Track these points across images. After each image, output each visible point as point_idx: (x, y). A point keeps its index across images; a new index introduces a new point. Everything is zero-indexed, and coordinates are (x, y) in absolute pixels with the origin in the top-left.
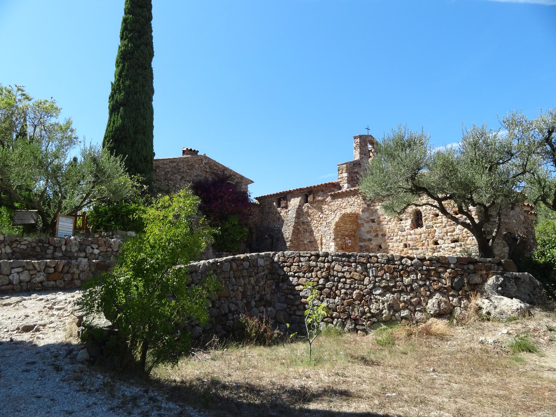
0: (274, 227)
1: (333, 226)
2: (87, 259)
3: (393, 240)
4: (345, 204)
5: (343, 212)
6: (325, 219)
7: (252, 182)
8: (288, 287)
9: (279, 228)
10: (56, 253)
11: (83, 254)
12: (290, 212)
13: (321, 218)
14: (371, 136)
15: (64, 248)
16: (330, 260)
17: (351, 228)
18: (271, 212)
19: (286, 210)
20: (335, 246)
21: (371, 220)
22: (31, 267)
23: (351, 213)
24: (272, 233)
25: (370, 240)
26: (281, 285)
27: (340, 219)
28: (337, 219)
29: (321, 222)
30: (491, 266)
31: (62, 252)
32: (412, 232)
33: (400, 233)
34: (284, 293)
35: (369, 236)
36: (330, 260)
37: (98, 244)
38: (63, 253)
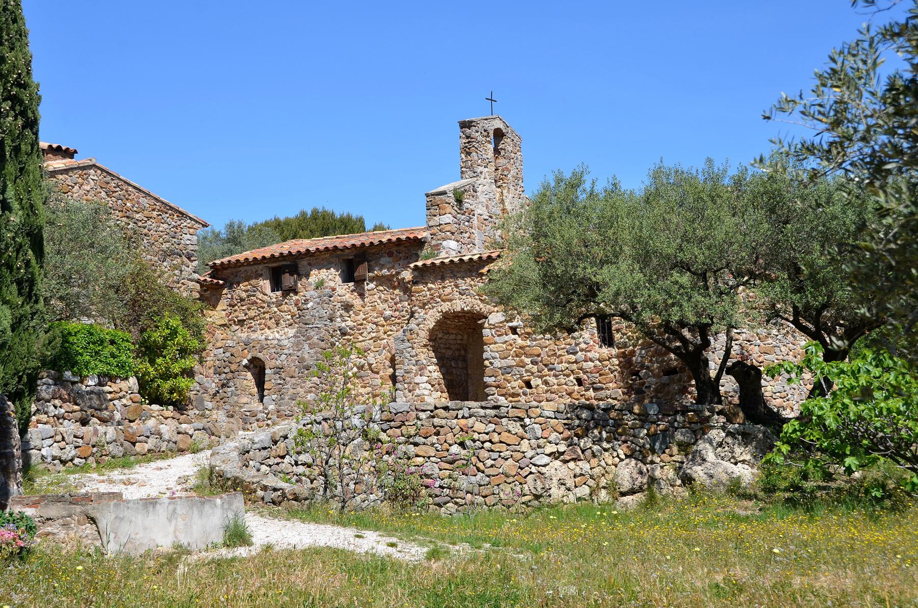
0: (266, 339)
5: (446, 307)
12: (310, 305)
13: (386, 319)
17: (459, 342)
19: (295, 298)
21: (511, 328)
24: (260, 355)
27: (439, 323)
28: (431, 325)
29: (388, 328)
36: (466, 415)
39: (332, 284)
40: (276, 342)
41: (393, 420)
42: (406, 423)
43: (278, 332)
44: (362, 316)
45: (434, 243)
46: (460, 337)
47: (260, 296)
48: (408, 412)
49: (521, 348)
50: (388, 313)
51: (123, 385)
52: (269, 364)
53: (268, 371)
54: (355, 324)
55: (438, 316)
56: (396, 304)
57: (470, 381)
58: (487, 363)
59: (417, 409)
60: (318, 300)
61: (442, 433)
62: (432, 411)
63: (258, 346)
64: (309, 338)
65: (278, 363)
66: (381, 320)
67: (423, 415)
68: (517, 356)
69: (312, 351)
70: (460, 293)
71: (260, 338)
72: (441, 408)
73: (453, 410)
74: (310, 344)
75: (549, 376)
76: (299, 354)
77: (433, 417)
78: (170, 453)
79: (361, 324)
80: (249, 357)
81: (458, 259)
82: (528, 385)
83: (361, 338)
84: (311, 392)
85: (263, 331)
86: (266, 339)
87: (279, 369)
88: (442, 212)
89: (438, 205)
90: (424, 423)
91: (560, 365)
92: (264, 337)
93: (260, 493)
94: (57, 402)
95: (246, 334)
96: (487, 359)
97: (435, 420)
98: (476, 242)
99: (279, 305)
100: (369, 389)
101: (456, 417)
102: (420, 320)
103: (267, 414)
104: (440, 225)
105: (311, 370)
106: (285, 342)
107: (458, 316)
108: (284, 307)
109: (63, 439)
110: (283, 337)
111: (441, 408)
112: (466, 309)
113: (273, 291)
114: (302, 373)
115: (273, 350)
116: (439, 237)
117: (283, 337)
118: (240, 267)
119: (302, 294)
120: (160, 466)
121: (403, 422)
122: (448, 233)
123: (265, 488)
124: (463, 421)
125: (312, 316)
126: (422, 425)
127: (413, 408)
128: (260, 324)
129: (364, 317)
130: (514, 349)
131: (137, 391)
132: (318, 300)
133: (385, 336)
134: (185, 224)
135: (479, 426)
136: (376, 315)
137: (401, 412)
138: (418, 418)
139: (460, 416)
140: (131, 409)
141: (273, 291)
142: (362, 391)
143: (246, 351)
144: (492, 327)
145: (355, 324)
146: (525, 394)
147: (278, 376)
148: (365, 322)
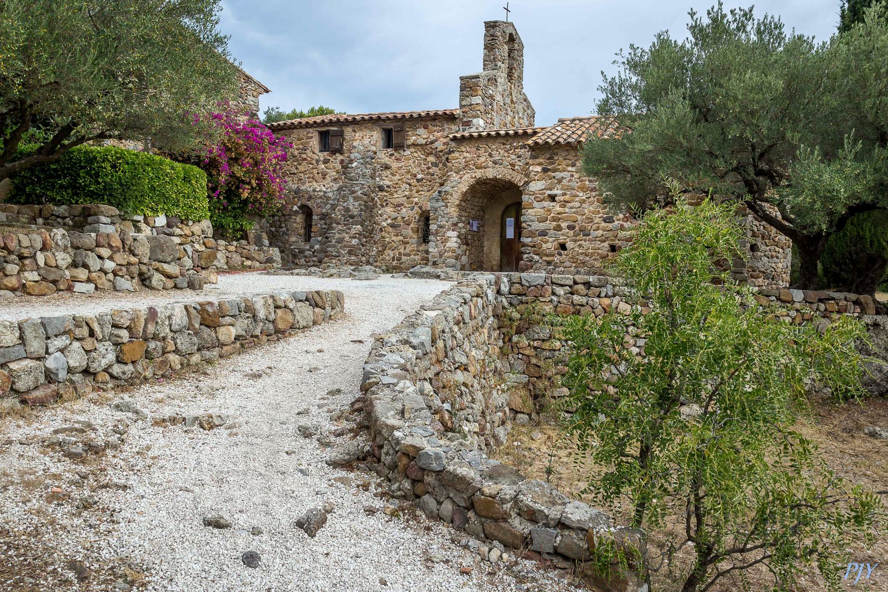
0: (314, 191)
1: (455, 199)
2: (93, 286)
3: (590, 237)
4: (483, 159)
5: (479, 174)
6: (429, 183)
7: (267, 91)
8: (532, 343)
9: (325, 192)
10: (26, 274)
11: (82, 274)
13: (418, 181)
14: (512, 24)
15: (41, 258)
16: (610, 294)
17: (481, 204)
18: (305, 159)
20: (458, 237)
21: (549, 196)
22: (85, 331)
23: (495, 179)
24: (309, 204)
25: (544, 233)
26: (515, 338)
30: (846, 306)
31: (38, 268)
32: (627, 225)
33: (603, 224)
34: (523, 355)
35: (542, 226)
36: (610, 294)
37: (110, 247)
38: (42, 272)
39: (374, 148)
40: (322, 194)
41: (525, 294)
42: (542, 299)
43: (324, 186)
44: (397, 177)
45: (465, 120)
46: (481, 200)
47: (310, 154)
48: (543, 286)
49: (558, 214)
50: (419, 176)
51: (196, 229)
52: (316, 210)
53: (315, 217)
54: (391, 183)
55: (472, 181)
56: (429, 168)
57: (485, 237)
58: (524, 225)
59: (553, 283)
60: (361, 161)
61: (582, 312)
62: (570, 287)
63: (307, 196)
64: (353, 192)
65: (324, 211)
66: (413, 182)
67: (560, 291)
68: (554, 221)
69: (356, 204)
70: (493, 162)
71: (308, 189)
72: (581, 283)
73: (596, 287)
74: (354, 197)
75: (585, 241)
76: (345, 204)
77: (572, 294)
78: (265, 338)
79: (397, 184)
80: (299, 204)
81: (477, 134)
82: (563, 247)
83: (396, 196)
84: (355, 238)
85: (311, 184)
86: (314, 191)
87: (324, 217)
88: (474, 93)
89: (471, 88)
90: (561, 300)
91: (596, 232)
92: (312, 188)
93: (519, 526)
94: (105, 252)
95: (296, 186)
96: (525, 222)
97: (575, 297)
98: (495, 123)
99: (326, 162)
100: (401, 238)
101: (599, 296)
102: (455, 183)
103: (314, 252)
104: (471, 105)
105: (356, 219)
106: (330, 195)
107: (486, 183)
108: (330, 165)
109: (92, 333)
110: (328, 190)
111: (581, 283)
112: (498, 177)
113: (321, 151)
114: (347, 221)
115: (319, 201)
116: (470, 115)
117: (328, 190)
118: (293, 129)
119: (346, 155)
120: (256, 368)
121: (537, 297)
122: (478, 112)
123: (532, 516)
124: (606, 301)
125: (357, 174)
126: (559, 302)
127: (549, 281)
128: (309, 178)
129: (399, 178)
130: (552, 215)
131: (211, 236)
132: (361, 161)
133: (416, 195)
134: (250, 87)
135: (624, 307)
136: (410, 177)
137: (535, 286)
138: (554, 294)
139: (603, 295)
140: (204, 255)
141: (321, 151)
142: (394, 238)
143: (296, 199)
144: (532, 193)
145: (391, 183)
146: (560, 254)
147: (323, 222)
148: (400, 182)
